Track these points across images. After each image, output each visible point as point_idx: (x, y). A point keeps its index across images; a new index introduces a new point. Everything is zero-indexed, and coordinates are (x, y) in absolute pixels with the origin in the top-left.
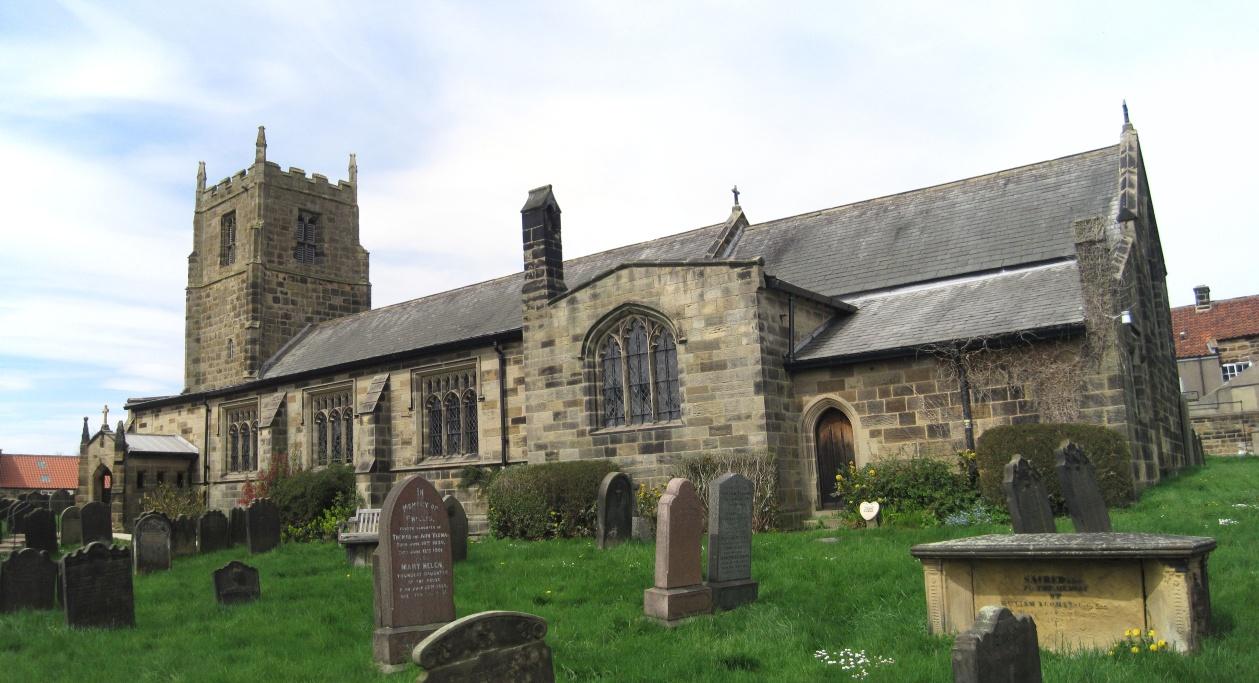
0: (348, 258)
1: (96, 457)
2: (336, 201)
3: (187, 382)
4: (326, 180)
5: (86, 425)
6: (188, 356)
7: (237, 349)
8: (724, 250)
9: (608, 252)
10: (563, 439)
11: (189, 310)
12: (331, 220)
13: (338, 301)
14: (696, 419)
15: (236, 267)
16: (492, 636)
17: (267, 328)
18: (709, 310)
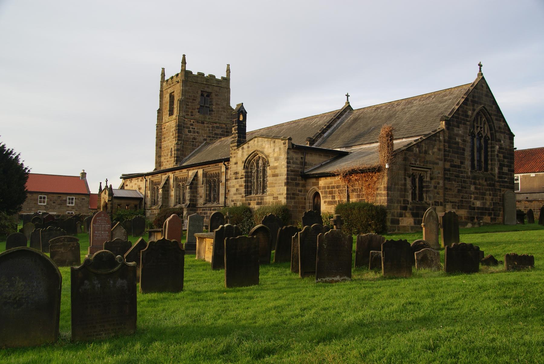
0: (224, 112)
1: (103, 198)
2: (219, 87)
3: (156, 166)
4: (214, 77)
5: (101, 185)
6: (156, 154)
7: (173, 152)
8: (336, 122)
9: (305, 118)
10: (238, 198)
11: (157, 134)
12: (216, 95)
13: (219, 131)
14: (270, 194)
15: (174, 116)
16: (66, 240)
17: (185, 144)
18: (276, 155)
